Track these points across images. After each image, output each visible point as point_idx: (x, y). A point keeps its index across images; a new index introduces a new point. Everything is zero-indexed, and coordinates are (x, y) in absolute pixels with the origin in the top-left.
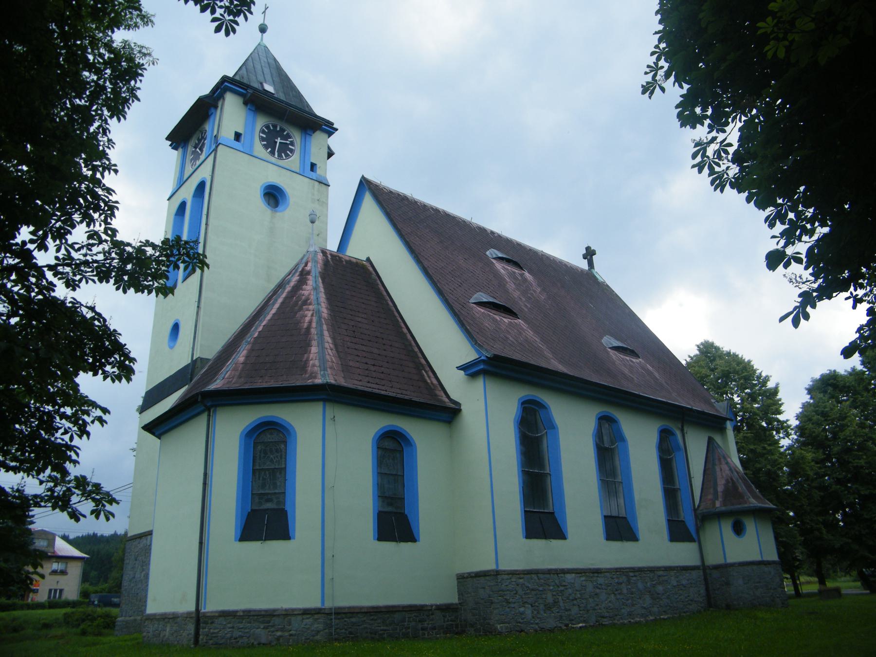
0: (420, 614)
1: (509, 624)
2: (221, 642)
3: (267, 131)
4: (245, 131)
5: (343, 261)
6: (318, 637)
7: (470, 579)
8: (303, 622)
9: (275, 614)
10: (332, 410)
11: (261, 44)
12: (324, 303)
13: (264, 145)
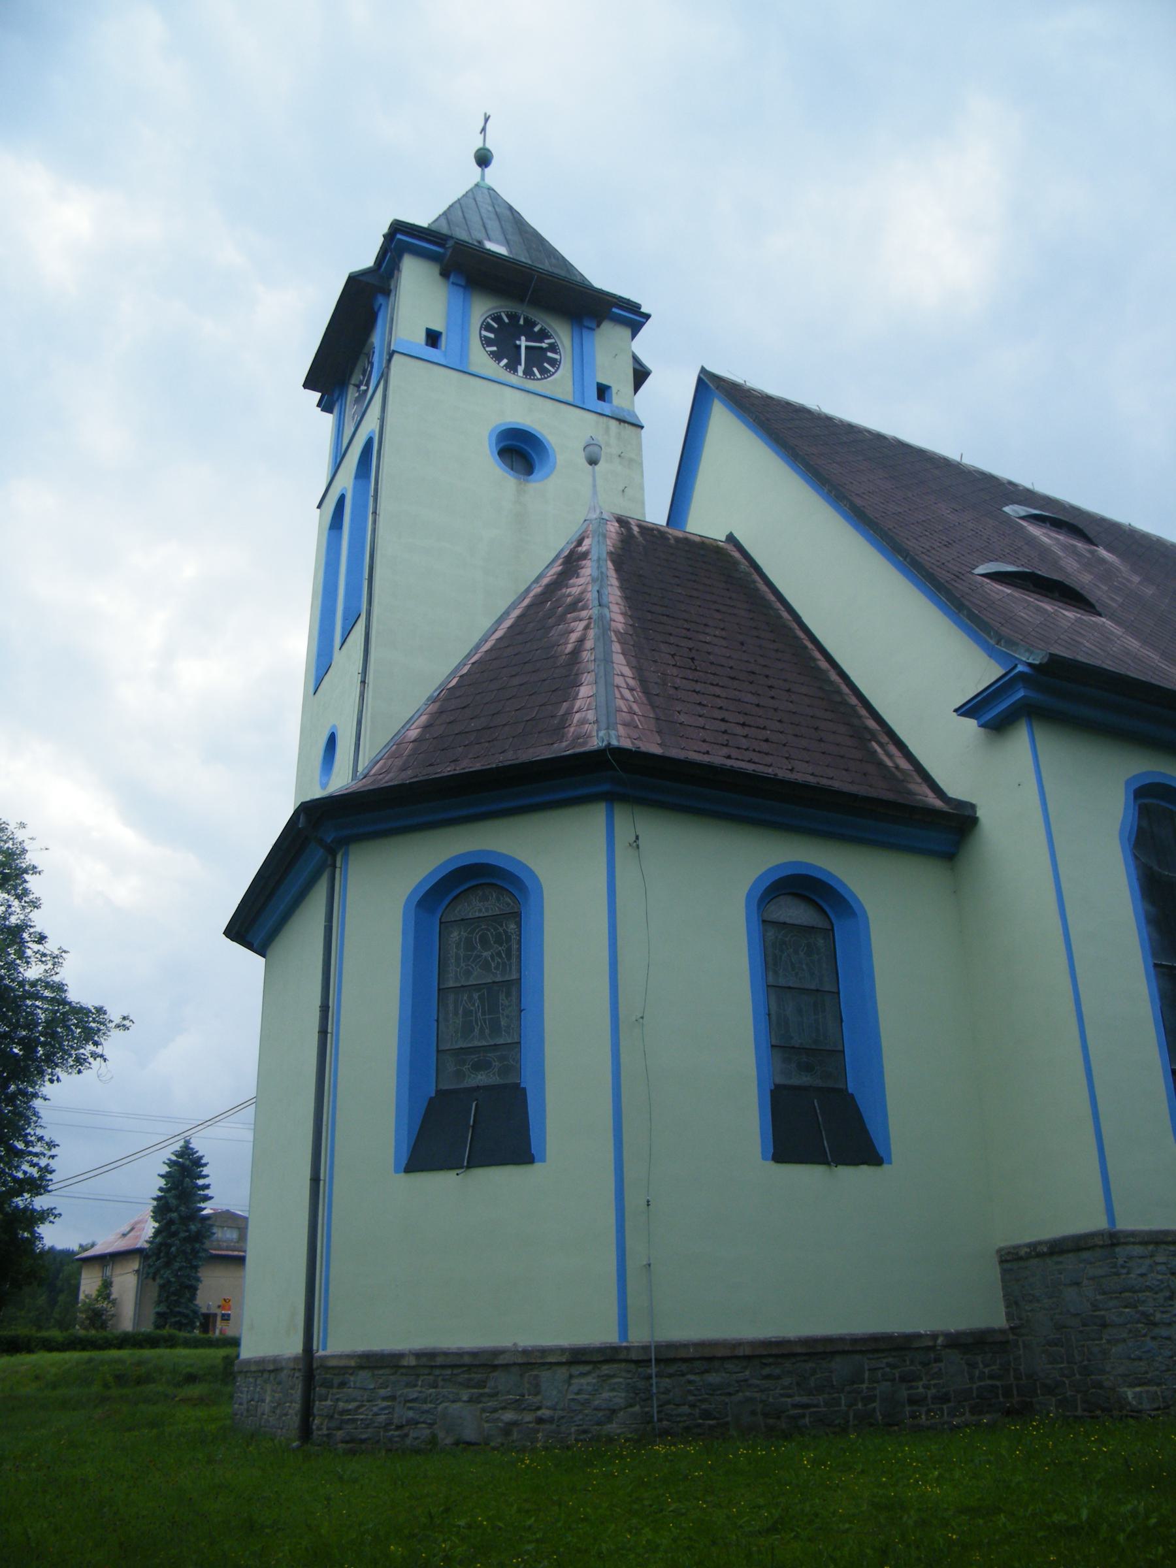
0: (905, 1361)
1: (1159, 1385)
2: (364, 1436)
3: (496, 326)
4: (448, 329)
5: (669, 539)
6: (613, 1428)
7: (1035, 1261)
8: (570, 1385)
9: (496, 1362)
10: (628, 823)
11: (482, 184)
12: (617, 604)
13: (492, 353)
